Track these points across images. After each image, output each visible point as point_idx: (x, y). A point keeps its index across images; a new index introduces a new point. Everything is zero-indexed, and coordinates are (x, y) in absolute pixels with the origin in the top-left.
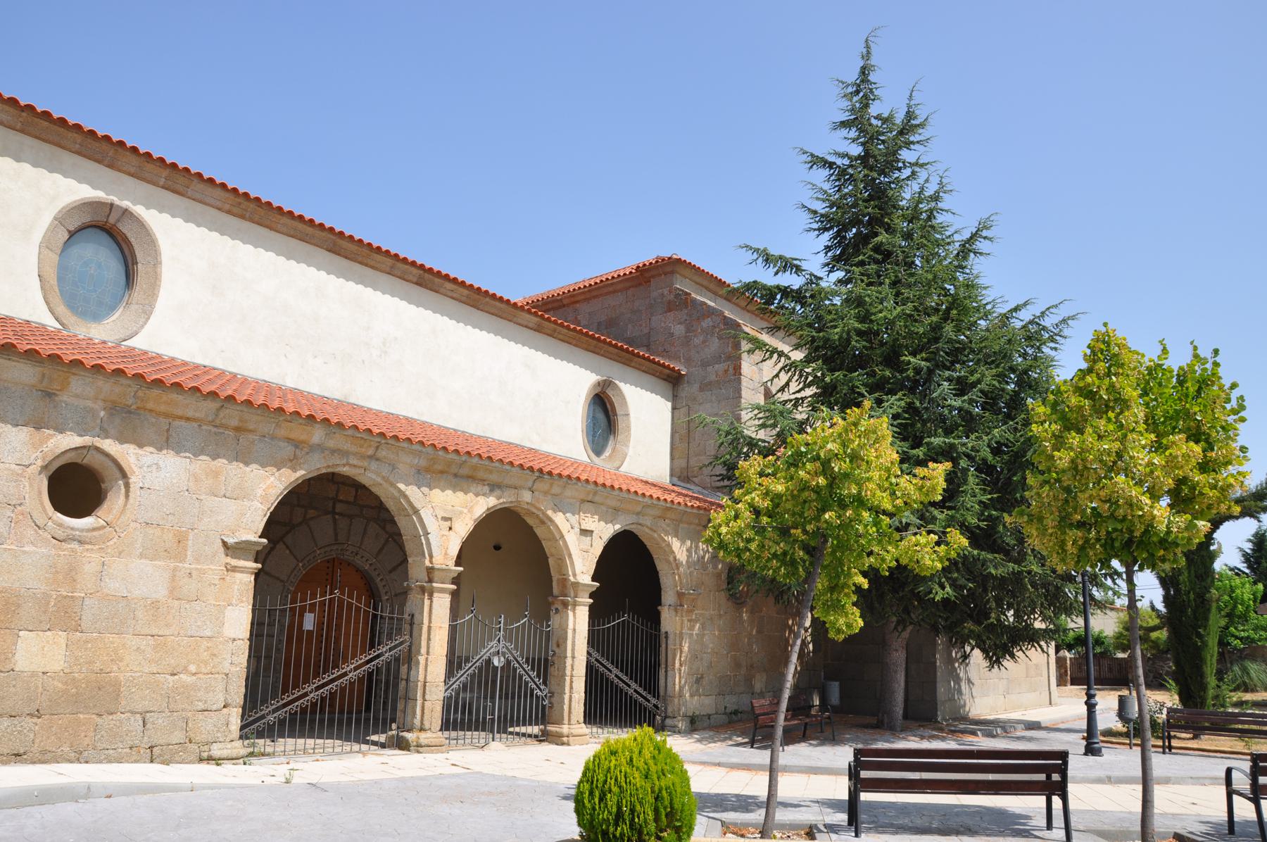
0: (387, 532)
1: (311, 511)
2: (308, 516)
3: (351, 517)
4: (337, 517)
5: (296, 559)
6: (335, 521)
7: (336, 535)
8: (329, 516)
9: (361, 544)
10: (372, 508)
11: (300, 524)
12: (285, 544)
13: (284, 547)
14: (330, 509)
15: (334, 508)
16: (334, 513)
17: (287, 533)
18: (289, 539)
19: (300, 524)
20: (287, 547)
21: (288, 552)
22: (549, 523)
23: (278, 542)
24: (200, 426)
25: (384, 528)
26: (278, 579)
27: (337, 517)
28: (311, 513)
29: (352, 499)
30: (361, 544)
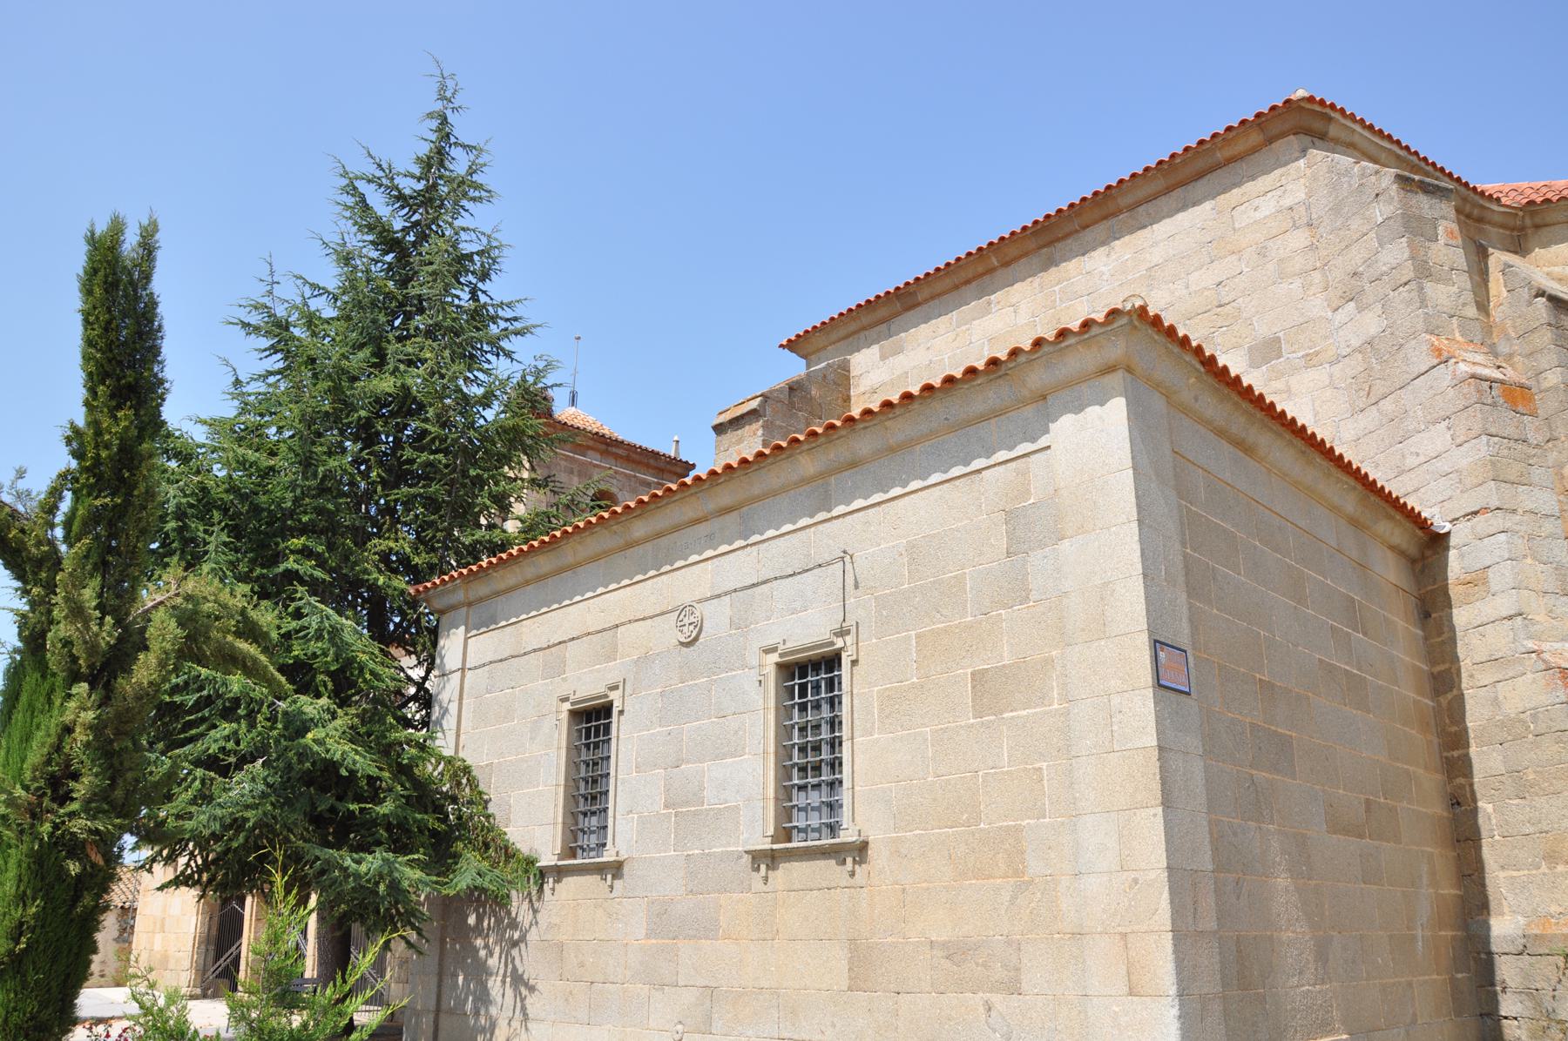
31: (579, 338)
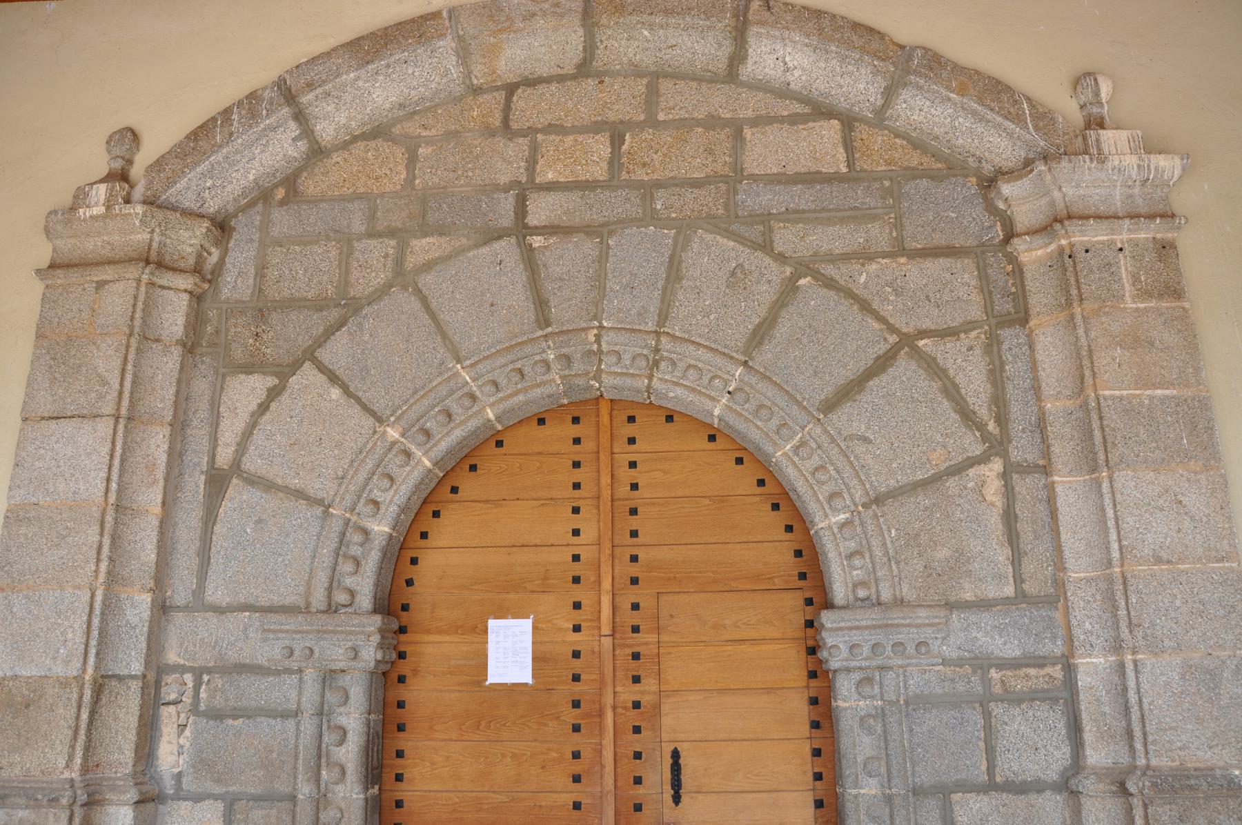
0: (781, 258)
1: (418, 244)
2: (411, 261)
3: (598, 231)
4: (537, 241)
5: (372, 413)
6: (529, 258)
7: (541, 304)
8: (506, 248)
9: (663, 318)
10: (696, 184)
11: (383, 291)
12: (322, 368)
13: (321, 378)
14: (507, 220)
15: (521, 210)
16: (521, 229)
17: (329, 333)
18: (337, 352)
19: (383, 291)
20: (333, 378)
21: (335, 393)
22: (227, 236)
23: (295, 366)
24: (601, 82)
25: (765, 246)
26: (300, 494)
27: (537, 241)
28: (424, 247)
29: (599, 172)
30: (663, 318)
31: (1087, 251)
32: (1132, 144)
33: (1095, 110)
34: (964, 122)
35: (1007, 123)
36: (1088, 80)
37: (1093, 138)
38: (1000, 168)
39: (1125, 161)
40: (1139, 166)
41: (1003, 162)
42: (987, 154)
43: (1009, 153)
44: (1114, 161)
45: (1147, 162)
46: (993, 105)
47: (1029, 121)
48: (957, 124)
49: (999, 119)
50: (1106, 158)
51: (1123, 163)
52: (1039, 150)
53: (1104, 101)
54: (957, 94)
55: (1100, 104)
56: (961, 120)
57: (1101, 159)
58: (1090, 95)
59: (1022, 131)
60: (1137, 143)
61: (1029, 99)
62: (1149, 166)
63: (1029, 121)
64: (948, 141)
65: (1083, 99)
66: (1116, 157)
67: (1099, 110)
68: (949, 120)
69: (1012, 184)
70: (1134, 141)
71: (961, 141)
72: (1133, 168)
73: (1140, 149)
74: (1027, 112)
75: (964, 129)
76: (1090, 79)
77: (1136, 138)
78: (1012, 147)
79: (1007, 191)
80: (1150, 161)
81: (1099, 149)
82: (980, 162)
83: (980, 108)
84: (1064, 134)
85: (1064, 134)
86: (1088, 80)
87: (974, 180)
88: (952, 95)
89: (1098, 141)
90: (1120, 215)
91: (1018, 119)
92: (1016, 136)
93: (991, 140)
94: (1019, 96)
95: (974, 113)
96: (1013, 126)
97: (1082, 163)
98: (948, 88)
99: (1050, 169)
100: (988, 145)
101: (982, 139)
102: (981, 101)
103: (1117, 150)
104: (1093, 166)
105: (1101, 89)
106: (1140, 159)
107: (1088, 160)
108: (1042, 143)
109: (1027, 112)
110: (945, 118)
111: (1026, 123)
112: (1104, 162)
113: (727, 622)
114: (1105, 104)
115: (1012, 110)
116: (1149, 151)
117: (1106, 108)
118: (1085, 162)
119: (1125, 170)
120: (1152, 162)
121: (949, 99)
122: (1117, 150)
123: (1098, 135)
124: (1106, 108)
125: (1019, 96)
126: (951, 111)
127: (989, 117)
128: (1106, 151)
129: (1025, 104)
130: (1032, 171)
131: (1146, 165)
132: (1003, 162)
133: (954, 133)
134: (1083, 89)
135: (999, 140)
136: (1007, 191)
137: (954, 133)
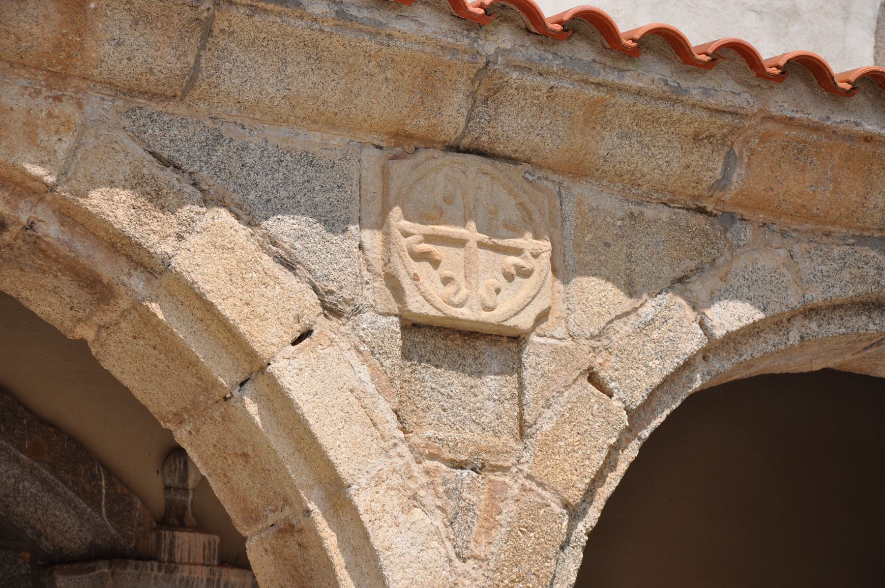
32: (206, 552)
33: (178, 497)
34: (30, 487)
35: (78, 501)
36: (177, 462)
37: (168, 541)
38: (61, 548)
39: (195, 573)
40: (208, 580)
41: (65, 542)
42: (49, 530)
43: (74, 532)
44: (184, 572)
45: (217, 576)
46: (66, 476)
47: (103, 503)
48: (21, 487)
49: (71, 494)
50: (175, 567)
51: (193, 575)
52: (108, 539)
53: (190, 487)
54: (29, 456)
55: (186, 490)
56: (27, 484)
57: (171, 566)
58: (177, 479)
59: (93, 513)
60: (212, 551)
61: (110, 473)
62: (219, 581)
63: (103, 503)
64: (7, 506)
65: (168, 481)
66: (187, 567)
67: (183, 498)
68: (13, 481)
69: (69, 577)
70: (210, 549)
71: (21, 509)
72: (202, 582)
73: (214, 559)
74: (104, 491)
75: (29, 494)
76: (180, 462)
77: (213, 545)
78: (80, 527)
79: (62, 584)
80: (220, 575)
81: (171, 554)
82: (38, 536)
83: (51, 477)
84: (140, 524)
85: (140, 524)
86: (177, 462)
87: (27, 555)
88: (23, 456)
89: (172, 544)
90: (658, 393)
91: (93, 499)
92: (86, 517)
93: (57, 513)
94: (99, 470)
95: (44, 482)
96: (85, 505)
97: (149, 571)
98: (20, 448)
99: (113, 574)
100: (52, 519)
101: (47, 511)
102: (54, 470)
103: (189, 557)
104: (160, 575)
105: (189, 477)
106: (212, 572)
107: (155, 569)
108: (113, 531)
109: (104, 491)
110: (8, 478)
111: (100, 506)
112: (172, 572)
113: (378, 434)
114: (190, 491)
115: (87, 487)
116: (223, 563)
117: (191, 497)
118: (152, 570)
119: (193, 583)
120: (223, 578)
121: (18, 460)
122: (189, 557)
123: (174, 537)
124: (191, 497)
125: (99, 470)
126: (17, 472)
127: (60, 490)
128: (178, 558)
129: (103, 481)
130: (93, 569)
131: (216, 580)
132: (65, 542)
133: (15, 498)
134: (171, 471)
135: (66, 516)
136: (62, 584)
137: (15, 498)
